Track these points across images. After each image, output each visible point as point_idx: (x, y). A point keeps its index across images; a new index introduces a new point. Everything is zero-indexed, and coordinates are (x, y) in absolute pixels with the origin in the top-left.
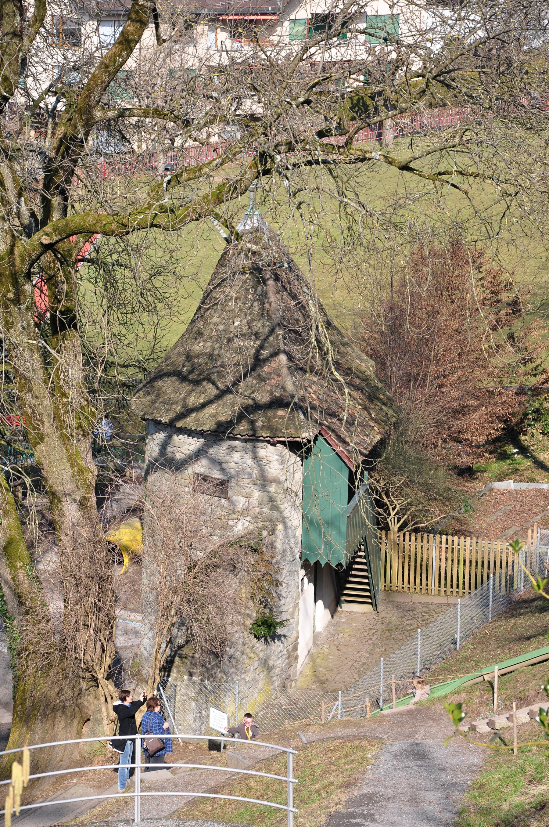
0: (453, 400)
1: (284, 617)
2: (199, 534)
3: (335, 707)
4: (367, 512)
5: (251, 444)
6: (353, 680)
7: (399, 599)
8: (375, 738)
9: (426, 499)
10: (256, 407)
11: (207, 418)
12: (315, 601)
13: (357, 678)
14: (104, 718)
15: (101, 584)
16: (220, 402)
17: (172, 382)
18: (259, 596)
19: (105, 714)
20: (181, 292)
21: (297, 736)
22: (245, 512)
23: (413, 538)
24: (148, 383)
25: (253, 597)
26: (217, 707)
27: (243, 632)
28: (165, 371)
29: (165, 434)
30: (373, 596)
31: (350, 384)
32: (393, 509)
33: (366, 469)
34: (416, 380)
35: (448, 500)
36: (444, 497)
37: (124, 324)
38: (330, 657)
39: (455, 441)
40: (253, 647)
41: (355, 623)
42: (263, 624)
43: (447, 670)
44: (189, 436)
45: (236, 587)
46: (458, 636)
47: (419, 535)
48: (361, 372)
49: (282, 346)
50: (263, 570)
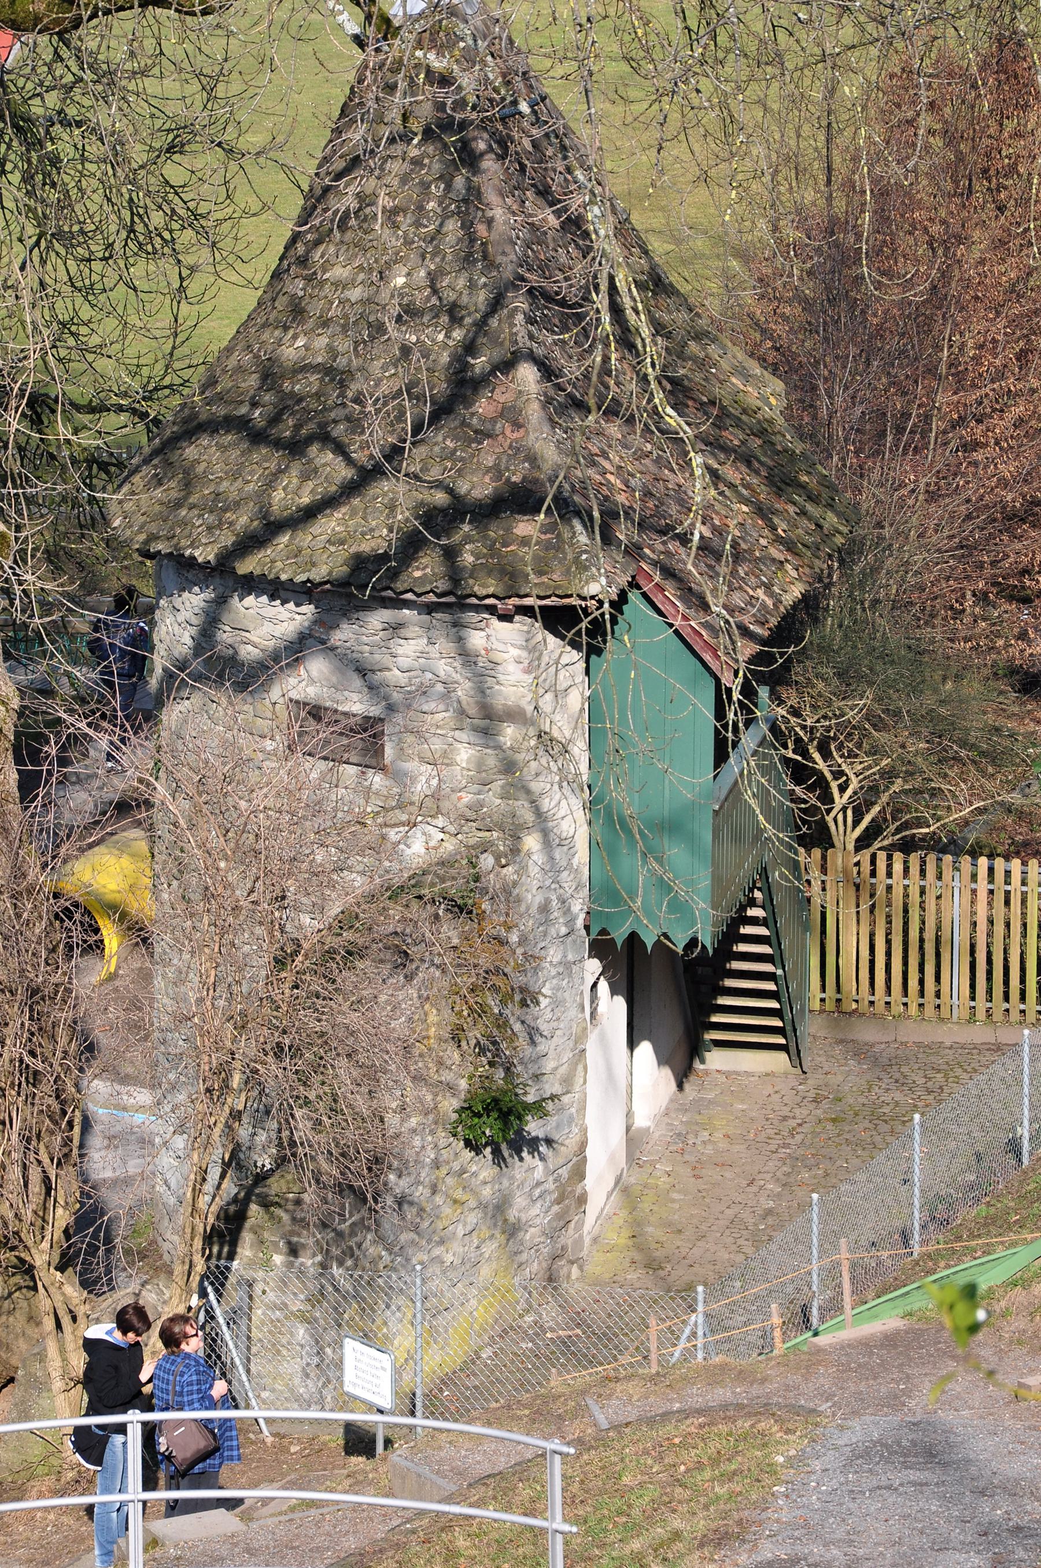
0: (1004, 483)
1: (552, 1087)
2: (304, 866)
3: (687, 1331)
4: (763, 795)
5: (446, 617)
6: (740, 1258)
7: (867, 1033)
8: (796, 1410)
9: (933, 759)
10: (459, 510)
11: (323, 549)
12: (632, 1044)
13: (749, 1250)
14: (54, 1374)
15: (36, 1008)
16: (356, 501)
17: (223, 448)
18: (475, 1034)
19: (58, 1363)
20: (244, 198)
21: (580, 1411)
22: (428, 802)
23: (898, 867)
24: (156, 453)
25: (457, 1037)
26: (366, 1338)
27: (432, 1133)
28: (203, 417)
29: (209, 595)
30: (789, 1028)
31: (712, 444)
32: (842, 789)
33: (762, 679)
34: (900, 430)
35: (993, 762)
36: (983, 754)
37: (88, 291)
38: (675, 1196)
39: (1011, 598)
40: (463, 1171)
41: (743, 1102)
42: (487, 1110)
43: (993, 1223)
44: (272, 597)
45: (410, 1010)
46: (1024, 1132)
47: (914, 859)
48: (745, 411)
49: (523, 340)
50: (485, 961)
